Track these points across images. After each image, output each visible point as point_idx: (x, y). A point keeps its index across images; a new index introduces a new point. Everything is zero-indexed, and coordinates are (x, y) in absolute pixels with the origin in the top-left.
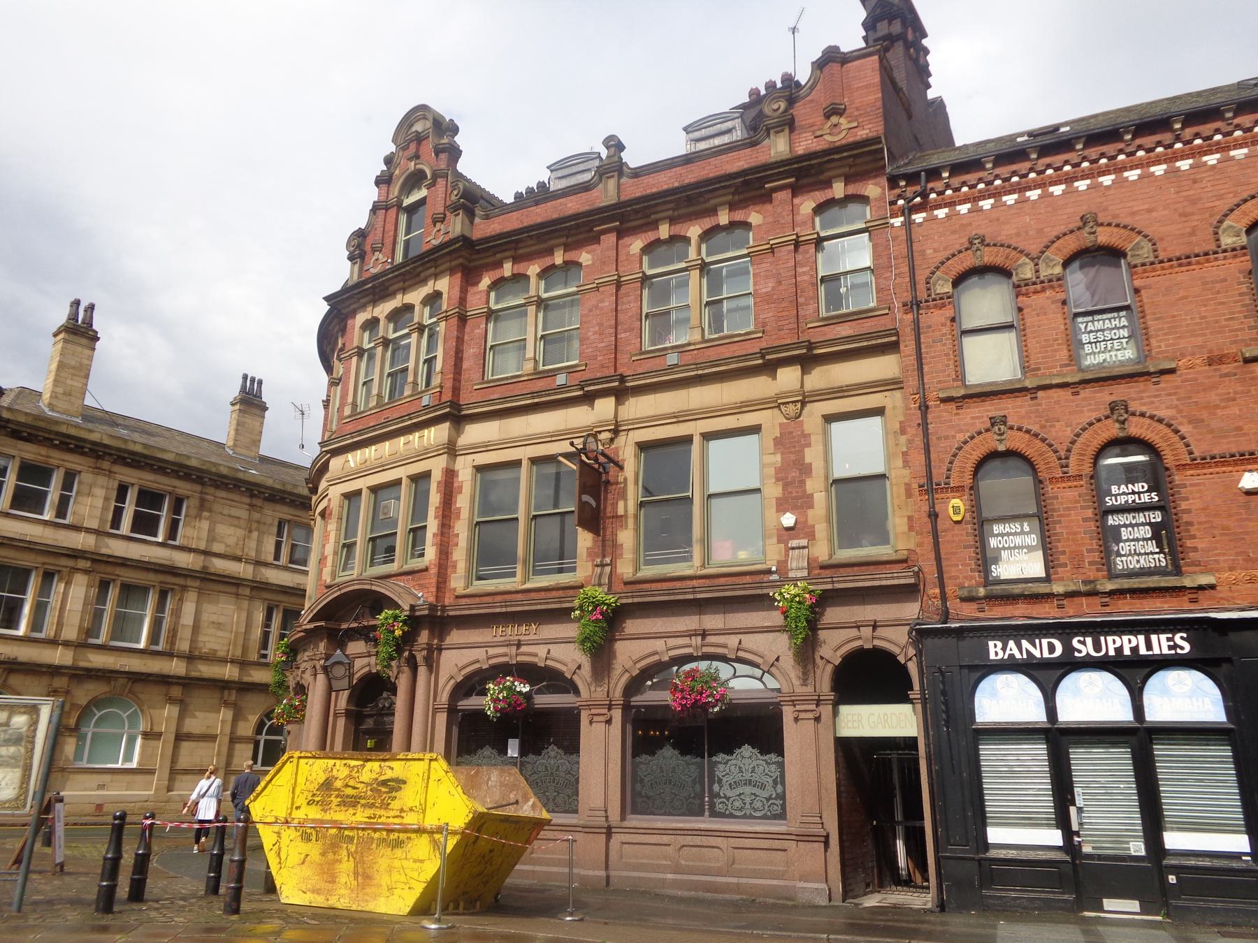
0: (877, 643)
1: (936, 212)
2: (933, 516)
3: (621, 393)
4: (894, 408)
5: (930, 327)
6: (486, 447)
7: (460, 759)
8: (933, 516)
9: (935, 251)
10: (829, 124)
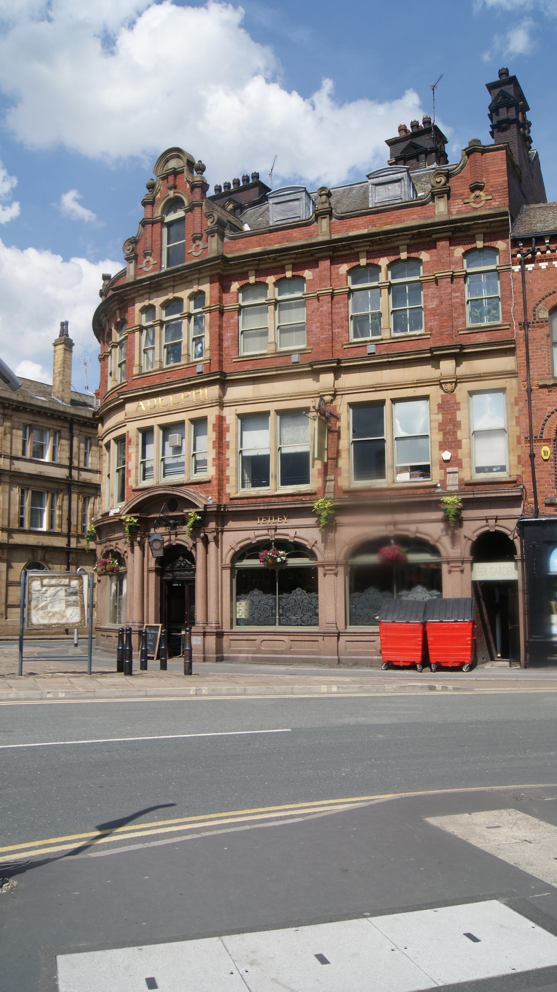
0: (498, 528)
1: (540, 264)
2: (532, 456)
3: (338, 370)
4: (512, 389)
5: (535, 339)
6: (245, 402)
7: (239, 597)
8: (532, 456)
9: (539, 290)
10: (474, 195)
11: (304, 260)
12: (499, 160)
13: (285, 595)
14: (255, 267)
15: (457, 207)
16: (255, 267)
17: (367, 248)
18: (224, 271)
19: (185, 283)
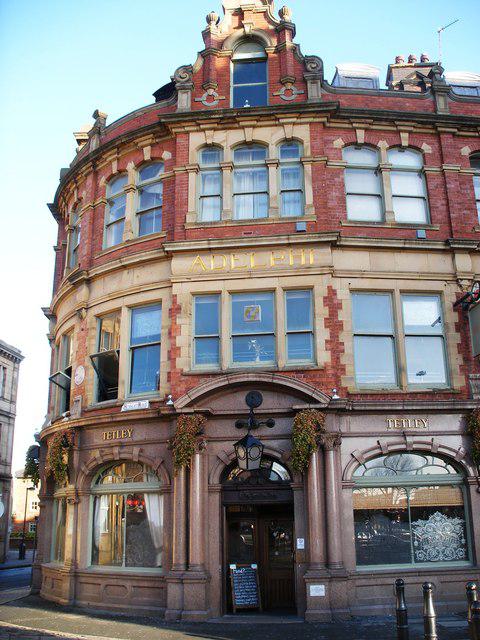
11: (424, 131)
19: (276, 125)
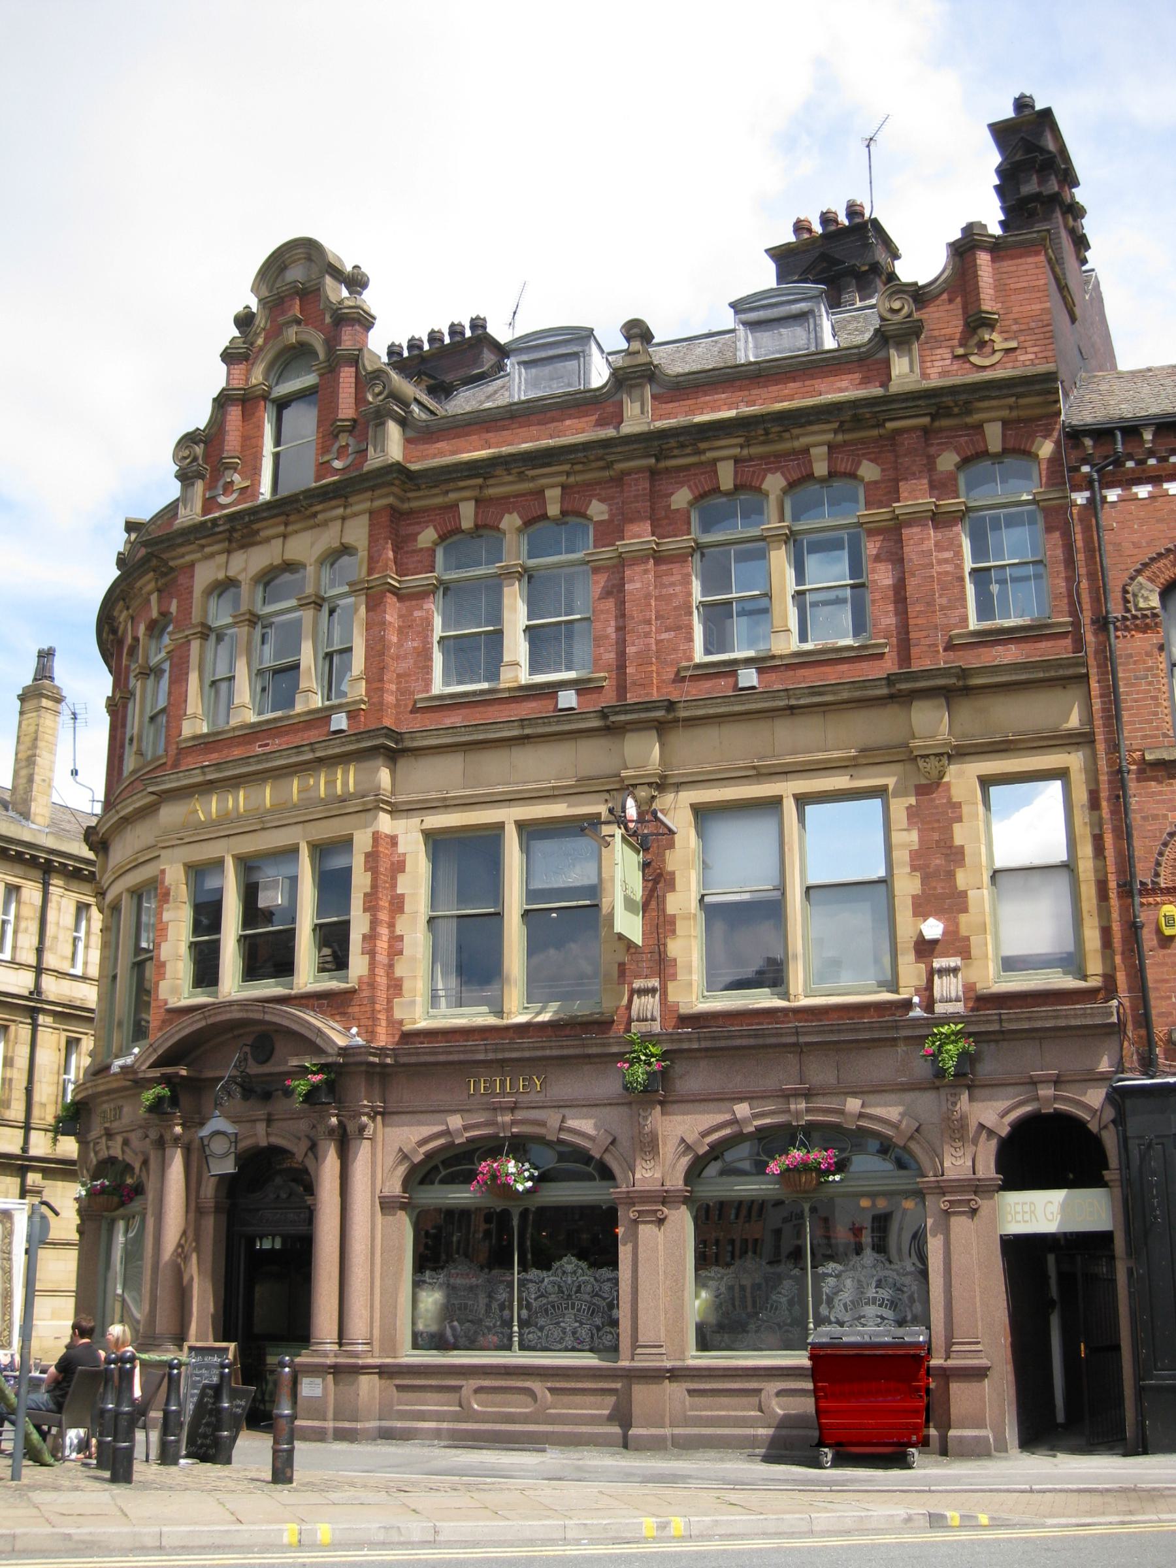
1: (1135, 489)
5: (1131, 656)
8: (1133, 929)
12: (1032, 266)
13: (534, 1274)
14: (475, 493)
15: (941, 363)
16: (475, 493)
17: (736, 451)
18: (402, 500)
19: (312, 527)
